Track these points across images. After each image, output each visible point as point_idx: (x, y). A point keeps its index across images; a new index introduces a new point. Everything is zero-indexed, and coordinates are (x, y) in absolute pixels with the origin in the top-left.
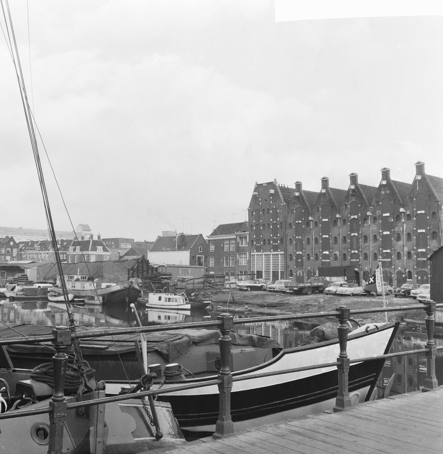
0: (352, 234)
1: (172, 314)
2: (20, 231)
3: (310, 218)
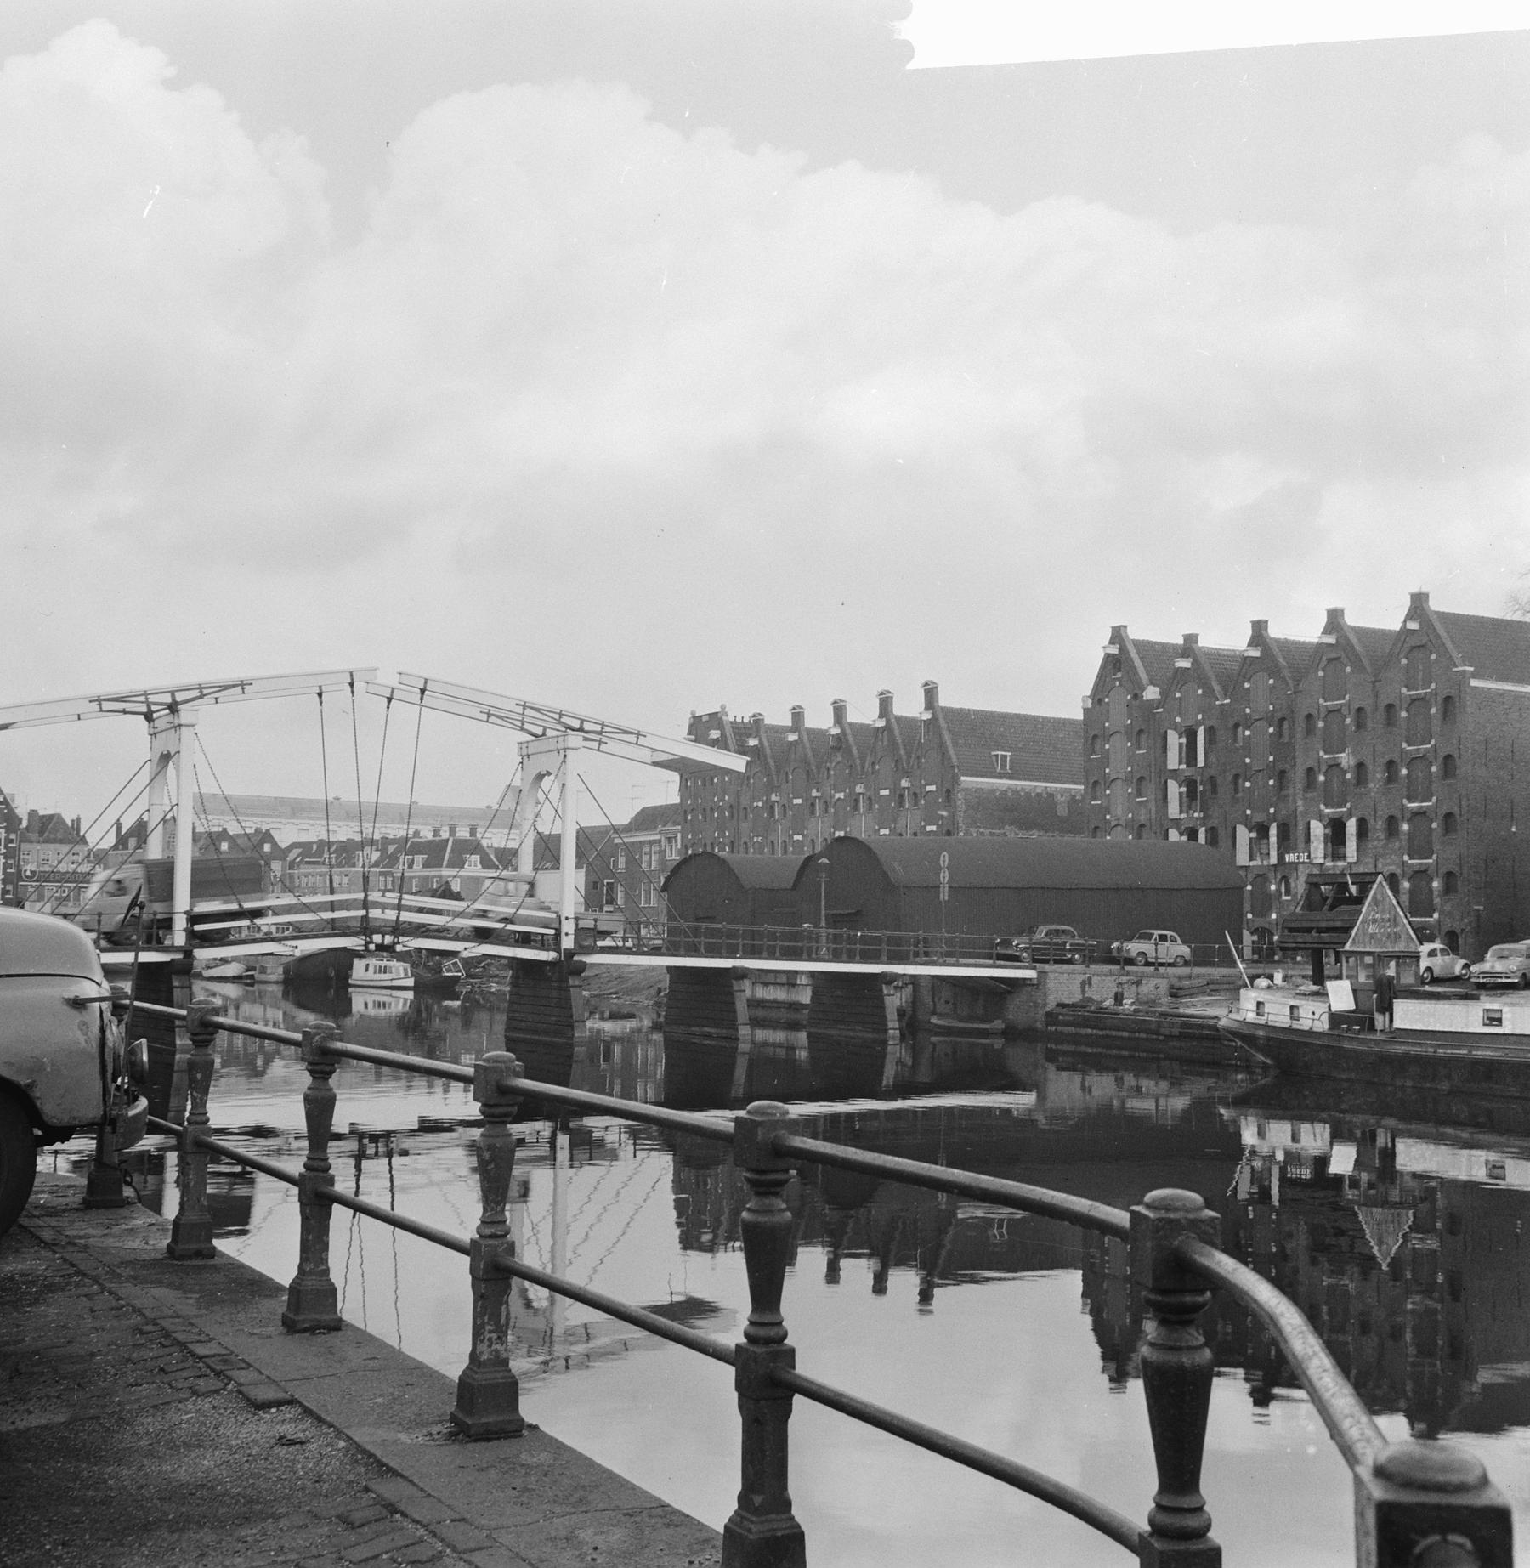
1: (383, 996)
2: (295, 809)
3: (904, 783)
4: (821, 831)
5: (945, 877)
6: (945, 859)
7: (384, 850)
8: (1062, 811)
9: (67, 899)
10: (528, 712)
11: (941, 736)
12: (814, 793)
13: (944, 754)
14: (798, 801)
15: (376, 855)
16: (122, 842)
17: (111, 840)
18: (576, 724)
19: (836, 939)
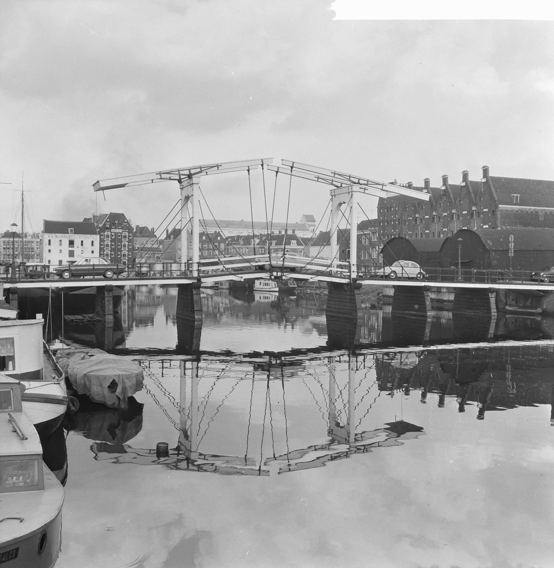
0: (444, 230)
2: (229, 224)
3: (474, 208)
4: (456, 226)
5: (512, 245)
6: (512, 238)
7: (261, 239)
8: (541, 219)
9: (150, 257)
10: (336, 176)
11: (490, 188)
12: (434, 213)
13: (492, 196)
14: (427, 217)
15: (257, 241)
16: (168, 237)
17: (164, 236)
18: (356, 181)
19: (465, 273)
